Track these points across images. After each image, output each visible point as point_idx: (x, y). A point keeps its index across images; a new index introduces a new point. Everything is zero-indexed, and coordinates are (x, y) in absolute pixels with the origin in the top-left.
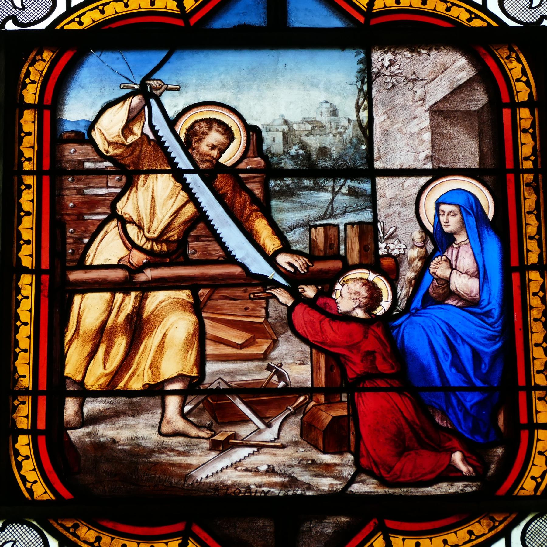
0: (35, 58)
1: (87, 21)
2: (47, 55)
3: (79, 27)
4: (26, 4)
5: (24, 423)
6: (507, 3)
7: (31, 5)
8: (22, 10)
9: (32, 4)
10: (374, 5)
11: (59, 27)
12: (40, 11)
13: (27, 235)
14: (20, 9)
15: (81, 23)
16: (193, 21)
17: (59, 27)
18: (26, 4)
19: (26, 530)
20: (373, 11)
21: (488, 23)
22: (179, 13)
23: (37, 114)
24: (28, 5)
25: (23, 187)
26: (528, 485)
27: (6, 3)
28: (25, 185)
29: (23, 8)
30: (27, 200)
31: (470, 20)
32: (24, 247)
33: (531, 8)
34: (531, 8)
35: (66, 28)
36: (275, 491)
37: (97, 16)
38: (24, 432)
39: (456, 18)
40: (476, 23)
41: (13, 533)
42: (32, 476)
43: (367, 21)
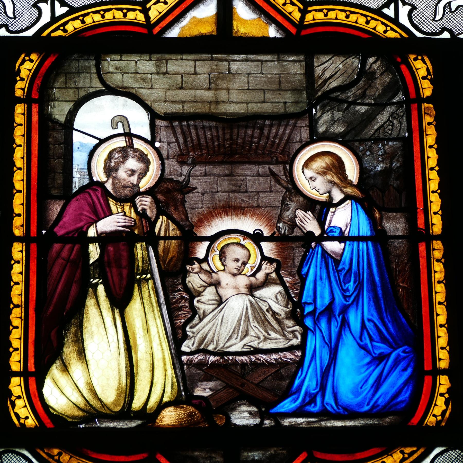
0: (24, 59)
1: (70, 28)
2: (34, 57)
3: (63, 34)
4: (17, 15)
5: (15, 367)
6: (17, 13)
7: (427, 7)
8: (13, 20)
9: (427, 8)
10: (305, 19)
11: (45, 34)
12: (29, 17)
13: (16, 343)
14: (12, 18)
15: (65, 31)
16: (157, 30)
17: (45, 34)
18: (17, 15)
19: (17, 459)
20: (305, 23)
21: (400, 35)
22: (145, 23)
23: (27, 107)
24: (424, 9)
25: (18, 78)
26: (431, 420)
27: (458, 24)
28: (20, 77)
29: (15, 18)
30: (14, 386)
31: (385, 32)
32: (16, 266)
33: (434, 20)
34: (434, 20)
35: (53, 35)
36: (136, 264)
37: (77, 24)
38: (16, 374)
39: (373, 29)
40: (391, 34)
41: (21, 16)
42: (23, 412)
43: (298, 32)
